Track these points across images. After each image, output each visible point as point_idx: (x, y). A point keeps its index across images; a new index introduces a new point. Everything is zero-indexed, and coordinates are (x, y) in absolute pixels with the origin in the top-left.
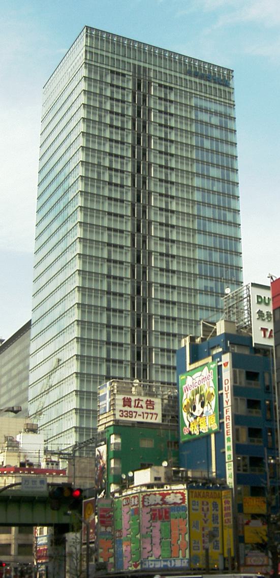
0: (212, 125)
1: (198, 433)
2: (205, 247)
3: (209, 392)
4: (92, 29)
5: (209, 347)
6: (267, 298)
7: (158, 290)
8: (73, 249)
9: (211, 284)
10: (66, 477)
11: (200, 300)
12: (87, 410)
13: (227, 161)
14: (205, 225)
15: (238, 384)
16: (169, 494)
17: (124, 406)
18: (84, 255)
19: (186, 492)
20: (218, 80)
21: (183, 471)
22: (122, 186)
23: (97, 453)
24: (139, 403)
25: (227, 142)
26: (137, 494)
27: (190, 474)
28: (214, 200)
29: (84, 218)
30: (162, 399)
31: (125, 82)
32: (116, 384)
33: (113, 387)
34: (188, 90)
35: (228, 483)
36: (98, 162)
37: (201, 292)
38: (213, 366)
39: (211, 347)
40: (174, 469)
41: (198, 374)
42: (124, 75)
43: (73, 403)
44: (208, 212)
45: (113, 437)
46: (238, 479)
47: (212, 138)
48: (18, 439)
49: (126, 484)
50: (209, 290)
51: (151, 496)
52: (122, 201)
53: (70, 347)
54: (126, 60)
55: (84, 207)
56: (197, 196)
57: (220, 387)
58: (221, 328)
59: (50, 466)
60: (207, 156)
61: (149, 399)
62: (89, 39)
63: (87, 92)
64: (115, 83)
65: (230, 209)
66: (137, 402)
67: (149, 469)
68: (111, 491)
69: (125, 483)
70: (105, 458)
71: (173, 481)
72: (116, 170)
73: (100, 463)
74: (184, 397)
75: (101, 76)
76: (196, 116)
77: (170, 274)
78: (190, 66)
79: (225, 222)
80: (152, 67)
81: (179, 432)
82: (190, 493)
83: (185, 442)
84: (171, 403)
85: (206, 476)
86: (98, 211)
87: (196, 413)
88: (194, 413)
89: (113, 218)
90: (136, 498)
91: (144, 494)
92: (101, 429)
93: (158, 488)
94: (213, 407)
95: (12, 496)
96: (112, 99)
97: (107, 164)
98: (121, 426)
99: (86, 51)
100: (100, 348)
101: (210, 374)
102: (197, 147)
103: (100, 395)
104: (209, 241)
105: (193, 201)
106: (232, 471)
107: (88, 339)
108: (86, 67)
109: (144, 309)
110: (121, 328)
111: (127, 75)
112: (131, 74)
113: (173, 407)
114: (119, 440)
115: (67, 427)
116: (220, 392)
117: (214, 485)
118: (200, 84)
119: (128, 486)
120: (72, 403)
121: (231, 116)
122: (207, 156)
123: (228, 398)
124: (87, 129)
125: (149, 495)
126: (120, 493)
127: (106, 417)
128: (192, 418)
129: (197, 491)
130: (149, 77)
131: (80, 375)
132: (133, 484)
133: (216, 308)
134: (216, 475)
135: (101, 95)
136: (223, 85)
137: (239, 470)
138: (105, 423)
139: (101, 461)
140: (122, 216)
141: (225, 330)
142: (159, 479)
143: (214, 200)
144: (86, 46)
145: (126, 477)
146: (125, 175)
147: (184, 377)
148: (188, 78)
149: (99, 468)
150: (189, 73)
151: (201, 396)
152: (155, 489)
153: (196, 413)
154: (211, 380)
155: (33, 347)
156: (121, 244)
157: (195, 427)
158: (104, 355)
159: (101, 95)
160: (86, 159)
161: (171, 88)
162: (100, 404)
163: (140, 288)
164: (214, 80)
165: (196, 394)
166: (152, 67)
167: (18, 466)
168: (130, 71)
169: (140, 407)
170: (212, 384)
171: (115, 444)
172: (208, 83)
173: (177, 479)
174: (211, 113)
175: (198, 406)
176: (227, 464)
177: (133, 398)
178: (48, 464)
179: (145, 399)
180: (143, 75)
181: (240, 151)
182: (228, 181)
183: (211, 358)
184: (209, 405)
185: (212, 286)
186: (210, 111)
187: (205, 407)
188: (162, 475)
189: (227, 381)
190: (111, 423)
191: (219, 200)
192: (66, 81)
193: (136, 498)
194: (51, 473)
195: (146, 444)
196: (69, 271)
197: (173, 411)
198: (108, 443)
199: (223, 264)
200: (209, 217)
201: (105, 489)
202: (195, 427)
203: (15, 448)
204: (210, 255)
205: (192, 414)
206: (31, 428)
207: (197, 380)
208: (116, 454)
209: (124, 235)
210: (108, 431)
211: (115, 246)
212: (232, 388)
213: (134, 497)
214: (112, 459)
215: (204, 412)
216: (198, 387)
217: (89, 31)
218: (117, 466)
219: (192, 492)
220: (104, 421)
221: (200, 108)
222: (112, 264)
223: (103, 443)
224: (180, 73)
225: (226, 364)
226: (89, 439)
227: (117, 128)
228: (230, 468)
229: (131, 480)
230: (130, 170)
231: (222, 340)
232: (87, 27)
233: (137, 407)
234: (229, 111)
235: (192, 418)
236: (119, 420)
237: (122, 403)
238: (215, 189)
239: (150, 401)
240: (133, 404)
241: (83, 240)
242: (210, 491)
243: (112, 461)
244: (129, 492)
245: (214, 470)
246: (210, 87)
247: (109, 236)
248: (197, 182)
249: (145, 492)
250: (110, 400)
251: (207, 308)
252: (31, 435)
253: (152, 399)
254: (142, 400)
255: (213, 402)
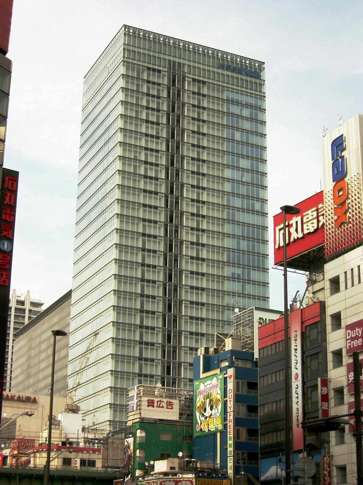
0: (243, 118)
1: (208, 431)
2: (234, 236)
3: (217, 398)
4: (129, 27)
5: (218, 360)
6: (268, 320)
7: (188, 277)
8: (112, 209)
9: (238, 271)
10: (101, 454)
11: (228, 286)
12: (120, 405)
13: (257, 152)
14: (234, 215)
15: (240, 393)
16: (181, 481)
17: (149, 406)
18: (119, 260)
19: (194, 480)
20: (247, 74)
21: (194, 461)
22: (157, 179)
23: (126, 443)
24: (160, 403)
25: (257, 134)
26: (156, 480)
27: (198, 465)
28: (243, 190)
29: (120, 225)
30: (180, 401)
31: (160, 78)
32: (142, 388)
33: (140, 390)
34: (220, 84)
35: (229, 474)
36: (135, 156)
37: (228, 279)
38: (221, 377)
39: (220, 360)
40: (186, 459)
41: (209, 382)
42: (159, 71)
43: (108, 398)
44: (237, 202)
45: (139, 431)
46: (237, 470)
47: (243, 130)
48: (59, 419)
49: (148, 470)
50: (236, 277)
51: (167, 482)
52: (156, 193)
53: (110, 238)
54: (162, 56)
55: (121, 200)
56: (227, 187)
57: (225, 395)
58: (229, 344)
59: (87, 444)
60: (238, 148)
61: (169, 400)
62: (127, 37)
63: (125, 90)
64: (151, 79)
65: (258, 199)
66: (159, 403)
67: (166, 460)
68: (136, 476)
69: (147, 469)
70: (132, 447)
71: (184, 470)
72: (151, 164)
73: (128, 452)
74: (198, 400)
75: (138, 73)
76: (228, 109)
77: (200, 262)
78: (223, 60)
79: (253, 212)
80: (187, 62)
81: (192, 429)
82: (197, 481)
83: (198, 437)
84: (187, 404)
85: (212, 467)
86: (133, 217)
87: (206, 414)
88: (205, 414)
89: (147, 209)
90: (155, 483)
91: (161, 480)
92: (130, 423)
93: (172, 476)
94: (219, 411)
95: (57, 476)
96: (148, 95)
97: (143, 158)
98: (146, 422)
99: (124, 49)
100: (134, 331)
101: (218, 384)
102: (228, 139)
103: (129, 396)
104: (238, 230)
105: (223, 192)
106: (232, 464)
107: (123, 307)
108: (124, 65)
109: (175, 295)
110: (153, 313)
111: (163, 71)
112: (166, 70)
113: (189, 407)
114: (143, 434)
115: (105, 402)
116: (225, 399)
117: (217, 474)
118: (233, 77)
119: (150, 473)
120: (107, 397)
121: (262, 108)
122: (238, 148)
123: (230, 404)
124: (125, 98)
125: (165, 482)
126: (143, 478)
127: (134, 415)
128: (203, 418)
129: (203, 480)
130: (183, 72)
131: (115, 356)
132: (154, 471)
133: (243, 294)
134: (220, 466)
135: (138, 91)
136: (255, 77)
137: (238, 463)
138: (133, 420)
139: (129, 450)
140: (156, 208)
141: (232, 346)
142: (174, 468)
143: (243, 190)
144: (124, 44)
145: (148, 464)
146: (159, 155)
147: (198, 383)
148: (220, 71)
149: (127, 456)
150: (221, 67)
151: (211, 401)
152: (170, 477)
153: (206, 414)
154: (218, 388)
155: (74, 311)
156: (155, 234)
157: (205, 425)
158: (138, 338)
159: (138, 78)
160: (123, 153)
161: (204, 83)
162: (129, 403)
163: (172, 275)
164: (246, 72)
165: (207, 399)
166: (187, 62)
167: (60, 445)
168: (165, 67)
169: (161, 407)
170: (219, 392)
171: (140, 437)
172: (239, 76)
173: (188, 469)
174: (242, 105)
175: (208, 409)
176: (228, 458)
177: (156, 400)
178: (85, 443)
179: (165, 400)
180: (178, 71)
181: (270, 142)
182: (257, 172)
183: (219, 370)
184: (216, 409)
185: (239, 273)
186: (241, 103)
187: (214, 410)
188: (176, 465)
189: (230, 391)
190: (137, 420)
191: (248, 190)
192: (105, 75)
193: (155, 483)
194: (88, 452)
195: (166, 437)
196: (108, 215)
197: (188, 410)
198: (134, 436)
199: (250, 252)
200: (238, 207)
201: (131, 473)
202: (205, 425)
203: (57, 427)
204: (238, 243)
205: (203, 415)
206: (71, 408)
207: (208, 386)
208: (141, 446)
209: (158, 226)
210: (135, 426)
211: (149, 236)
212: (235, 395)
213: (154, 482)
214: (138, 449)
215: (213, 414)
216: (208, 393)
217: (127, 30)
218: (141, 455)
219: (199, 480)
220: (132, 418)
221: (231, 101)
222: (147, 238)
223: (131, 436)
224: (214, 67)
225: (230, 377)
226: (121, 429)
227: (152, 123)
228: (230, 461)
229: (153, 467)
230: (164, 163)
231: (229, 356)
232: (125, 26)
233: (159, 407)
234: (259, 102)
235: (203, 418)
236: (143, 418)
237: (147, 404)
238: (244, 180)
239: (170, 402)
240: (155, 404)
241: (120, 216)
242: (213, 480)
243: (138, 451)
244: (150, 478)
245: (219, 462)
246: (242, 79)
247: (144, 226)
248: (228, 173)
249: (162, 478)
250: (137, 400)
251: (233, 294)
252: (71, 415)
253: (171, 401)
254: (164, 402)
255: (220, 407)
